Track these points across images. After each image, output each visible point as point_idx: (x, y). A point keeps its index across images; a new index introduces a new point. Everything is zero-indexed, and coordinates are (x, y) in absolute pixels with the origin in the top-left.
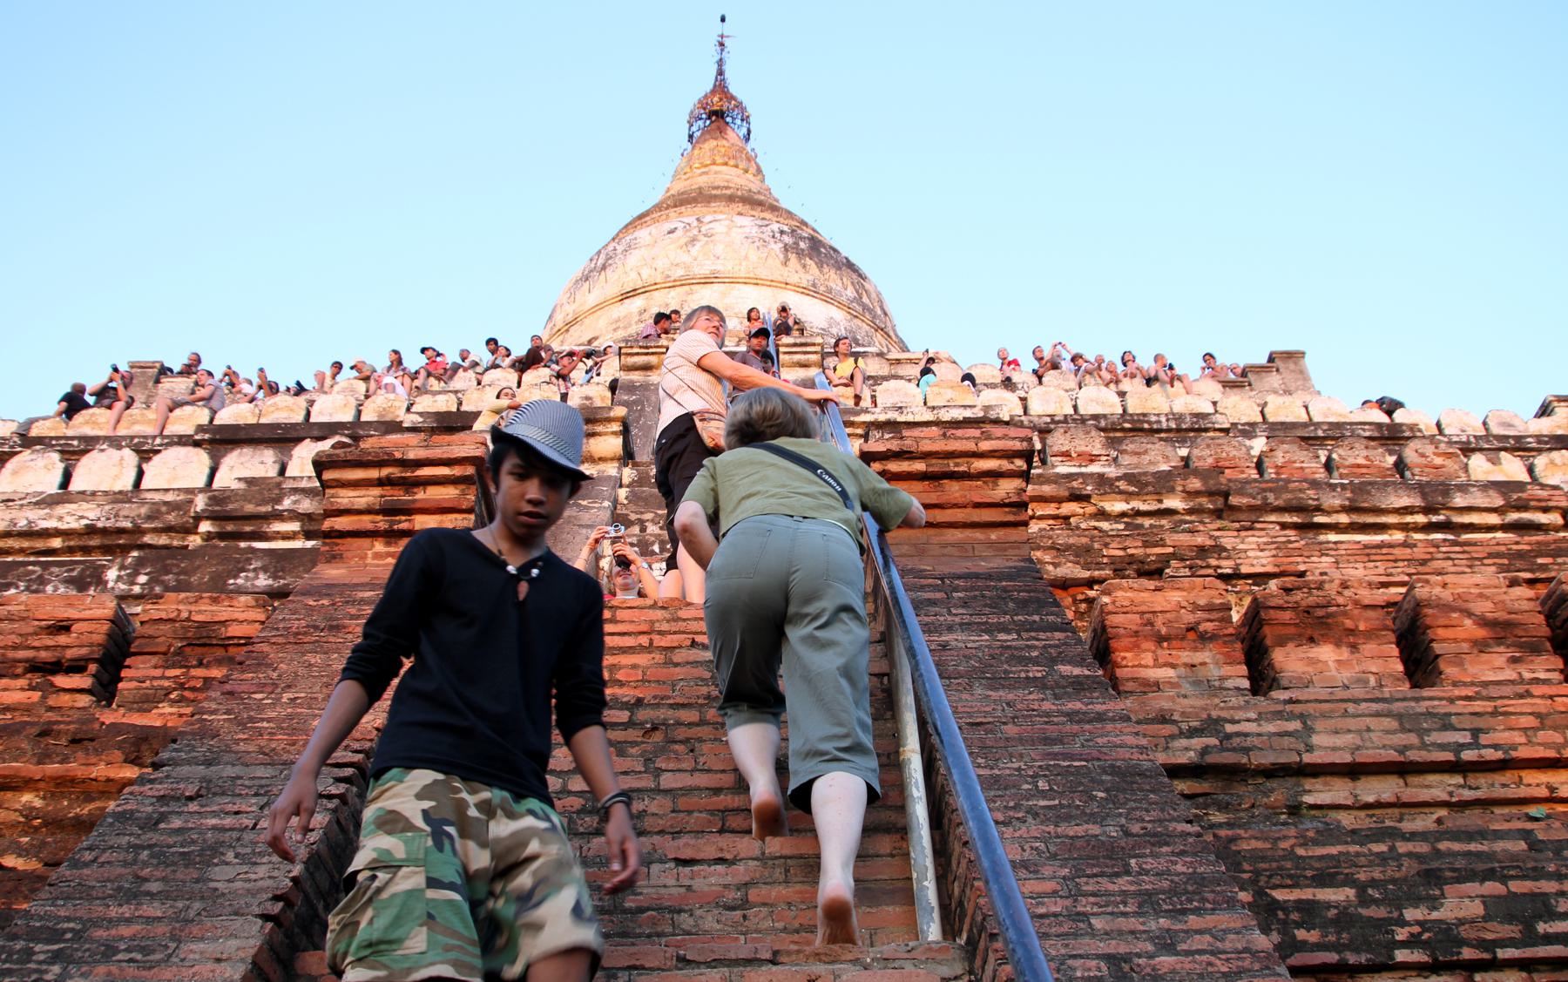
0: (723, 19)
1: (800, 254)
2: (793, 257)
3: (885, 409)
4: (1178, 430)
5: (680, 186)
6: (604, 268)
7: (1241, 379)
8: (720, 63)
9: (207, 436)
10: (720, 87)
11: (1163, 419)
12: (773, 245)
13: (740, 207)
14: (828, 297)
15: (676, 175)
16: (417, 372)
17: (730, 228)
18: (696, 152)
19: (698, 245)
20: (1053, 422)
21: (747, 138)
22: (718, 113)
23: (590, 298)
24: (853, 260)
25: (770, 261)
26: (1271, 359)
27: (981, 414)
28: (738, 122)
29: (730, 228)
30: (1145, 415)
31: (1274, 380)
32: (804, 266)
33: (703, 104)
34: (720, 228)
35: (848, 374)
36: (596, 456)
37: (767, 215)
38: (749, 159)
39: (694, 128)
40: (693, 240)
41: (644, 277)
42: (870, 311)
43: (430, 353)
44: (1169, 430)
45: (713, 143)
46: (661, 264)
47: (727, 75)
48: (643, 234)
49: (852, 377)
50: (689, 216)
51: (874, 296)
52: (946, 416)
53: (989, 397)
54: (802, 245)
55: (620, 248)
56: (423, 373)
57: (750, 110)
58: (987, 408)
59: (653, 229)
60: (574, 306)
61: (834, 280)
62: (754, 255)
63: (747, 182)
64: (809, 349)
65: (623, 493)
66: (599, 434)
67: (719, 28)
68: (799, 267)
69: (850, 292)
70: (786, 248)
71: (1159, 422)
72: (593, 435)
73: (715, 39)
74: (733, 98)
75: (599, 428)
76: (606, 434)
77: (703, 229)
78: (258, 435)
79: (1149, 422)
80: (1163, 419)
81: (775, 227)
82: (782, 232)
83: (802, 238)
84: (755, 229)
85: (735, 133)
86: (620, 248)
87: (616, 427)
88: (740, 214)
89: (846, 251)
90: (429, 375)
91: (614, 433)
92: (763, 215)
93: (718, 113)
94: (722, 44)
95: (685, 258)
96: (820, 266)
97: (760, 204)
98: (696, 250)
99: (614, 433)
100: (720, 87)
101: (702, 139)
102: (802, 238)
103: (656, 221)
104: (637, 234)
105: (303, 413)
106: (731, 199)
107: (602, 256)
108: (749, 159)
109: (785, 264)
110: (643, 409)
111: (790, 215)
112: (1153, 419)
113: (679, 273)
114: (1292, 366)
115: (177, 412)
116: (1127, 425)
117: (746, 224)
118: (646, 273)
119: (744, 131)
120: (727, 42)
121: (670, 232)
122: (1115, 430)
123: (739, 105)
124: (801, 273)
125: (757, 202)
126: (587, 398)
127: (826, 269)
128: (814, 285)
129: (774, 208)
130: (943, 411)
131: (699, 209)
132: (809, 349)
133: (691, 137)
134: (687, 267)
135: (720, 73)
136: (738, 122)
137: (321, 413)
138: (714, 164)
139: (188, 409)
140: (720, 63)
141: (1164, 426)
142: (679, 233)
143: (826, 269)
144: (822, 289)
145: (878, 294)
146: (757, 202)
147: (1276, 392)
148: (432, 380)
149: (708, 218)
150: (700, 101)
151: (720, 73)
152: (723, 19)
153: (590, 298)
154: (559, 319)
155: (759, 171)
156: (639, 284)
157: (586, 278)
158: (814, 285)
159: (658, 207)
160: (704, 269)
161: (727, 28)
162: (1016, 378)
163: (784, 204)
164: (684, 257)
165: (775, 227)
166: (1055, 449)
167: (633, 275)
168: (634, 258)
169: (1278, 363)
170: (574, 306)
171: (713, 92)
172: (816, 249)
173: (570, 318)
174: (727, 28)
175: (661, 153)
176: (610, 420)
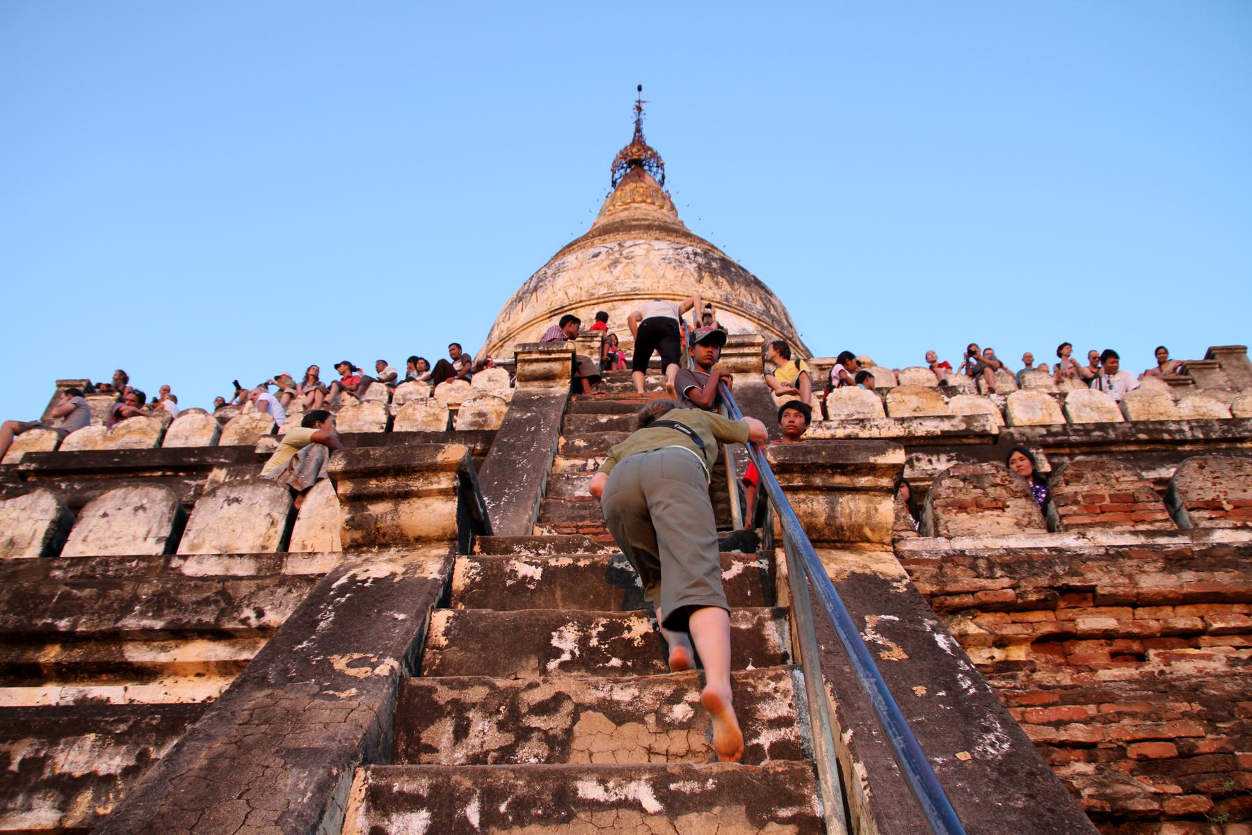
0: (640, 89)
1: (713, 273)
2: (706, 276)
3: (843, 423)
4: (1207, 441)
5: (604, 221)
6: (535, 289)
7: (1181, 377)
8: (638, 123)
9: (33, 466)
10: (638, 140)
11: (1186, 428)
12: (688, 265)
13: (657, 234)
14: (740, 310)
15: (602, 213)
16: (330, 388)
17: (648, 251)
18: (619, 193)
19: (620, 267)
20: (1050, 434)
21: (662, 183)
22: (637, 162)
23: (522, 316)
24: (760, 278)
25: (686, 279)
26: (1211, 354)
27: (963, 427)
28: (655, 169)
29: (648, 251)
30: (1161, 423)
31: (1218, 377)
32: (717, 283)
33: (624, 155)
34: (639, 251)
35: (792, 380)
36: (411, 535)
37: (682, 240)
38: (664, 198)
39: (617, 176)
40: (615, 263)
41: (571, 295)
42: (779, 322)
43: (343, 367)
44: (1195, 441)
45: (633, 185)
46: (587, 283)
47: (644, 132)
48: (571, 259)
49: (797, 384)
50: (612, 242)
51: (780, 309)
52: (921, 429)
53: (962, 405)
54: (714, 265)
55: (550, 272)
56: (335, 388)
57: (664, 159)
58: (968, 419)
59: (579, 254)
60: (508, 324)
61: (744, 295)
62: (670, 274)
63: (661, 215)
64: (746, 350)
65: (440, 619)
66: (418, 495)
67: (636, 95)
68: (712, 284)
69: (759, 306)
70: (700, 268)
71: (1181, 431)
72: (407, 495)
73: (634, 104)
74: (650, 149)
75: (418, 484)
76: (429, 494)
77: (624, 253)
78: (91, 464)
79: (1169, 432)
80: (1186, 428)
81: (689, 249)
82: (696, 254)
83: (714, 259)
84: (671, 251)
85: (651, 178)
86: (550, 272)
87: (445, 481)
88: (657, 239)
89: (753, 270)
90: (341, 389)
91: (443, 492)
92: (677, 240)
93: (637, 162)
94: (639, 109)
95: (608, 278)
96: (731, 283)
97: (676, 231)
98: (617, 271)
99: (443, 492)
100: (638, 140)
101: (624, 183)
102: (714, 259)
103: (581, 247)
104: (565, 259)
105: (156, 436)
106: (649, 228)
107: (535, 280)
108: (664, 198)
109: (700, 280)
110: (537, 431)
111: (702, 241)
112: (1173, 427)
113: (603, 291)
114: (1235, 362)
115: (24, 436)
116: (1142, 436)
117: (664, 247)
118: (572, 292)
119: (659, 177)
120: (643, 106)
121: (596, 256)
122: (1128, 443)
123: (655, 155)
124: (715, 289)
125: (672, 230)
126: (481, 414)
127: (737, 286)
128: (727, 300)
129: (687, 235)
130: (915, 424)
131: (620, 236)
132: (746, 350)
133: (614, 183)
134: (609, 286)
135: (638, 130)
136: (655, 169)
137: (176, 436)
138: (634, 201)
139: (35, 432)
140: (638, 123)
141: (1189, 435)
142: (602, 257)
143: (737, 286)
144: (735, 303)
145: (783, 308)
146: (672, 230)
147: (1224, 390)
148: (345, 395)
149: (629, 243)
150: (621, 153)
151: (638, 130)
152: (640, 89)
153: (522, 316)
154: (495, 339)
155: (673, 208)
156: (566, 302)
157: (520, 299)
158: (727, 300)
159: (585, 237)
160: (626, 286)
161: (643, 96)
162: (952, 381)
163: (694, 232)
164: (608, 278)
165: (689, 249)
166: (1193, 496)
167: (561, 294)
168: (562, 280)
169: (1219, 359)
170: (508, 324)
171: (633, 145)
172: (727, 269)
173: (504, 334)
174: (643, 96)
175: (590, 193)
176: (436, 469)
